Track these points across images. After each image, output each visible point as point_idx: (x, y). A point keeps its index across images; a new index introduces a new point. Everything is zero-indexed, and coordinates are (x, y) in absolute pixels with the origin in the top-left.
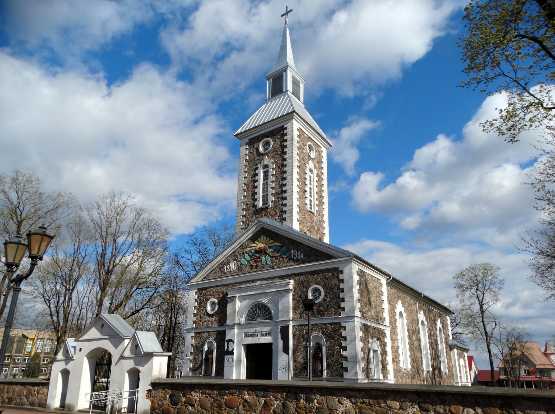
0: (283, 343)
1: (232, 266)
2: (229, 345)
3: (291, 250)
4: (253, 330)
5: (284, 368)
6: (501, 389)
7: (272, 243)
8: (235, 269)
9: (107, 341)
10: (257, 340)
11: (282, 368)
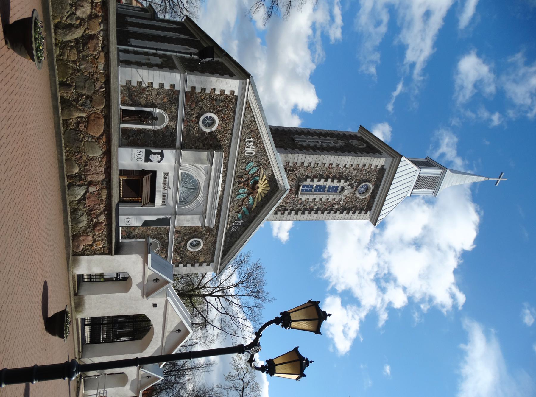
0: (154, 221)
1: (251, 150)
2: (157, 155)
3: (243, 220)
4: (171, 184)
5: (129, 222)
6: (114, 175)
7: (258, 200)
8: (246, 154)
9: (160, 344)
10: (160, 190)
11: (129, 219)
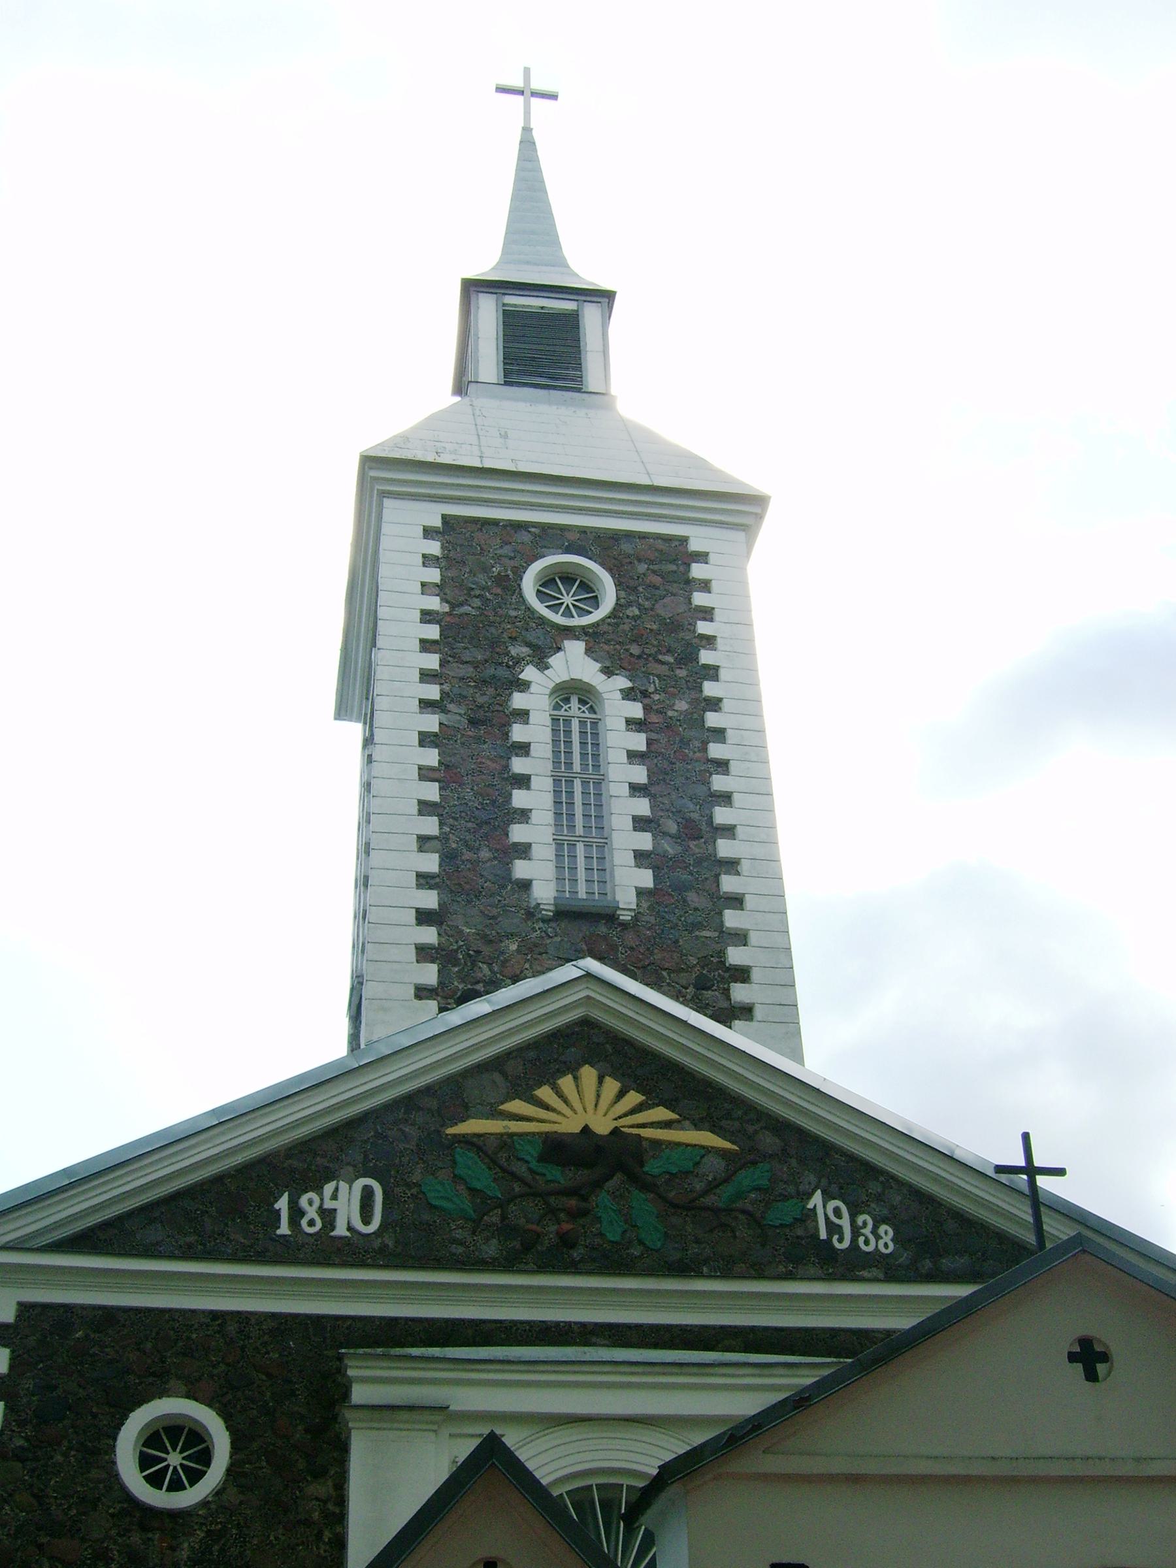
3: (810, 1195)
7: (667, 1125)
